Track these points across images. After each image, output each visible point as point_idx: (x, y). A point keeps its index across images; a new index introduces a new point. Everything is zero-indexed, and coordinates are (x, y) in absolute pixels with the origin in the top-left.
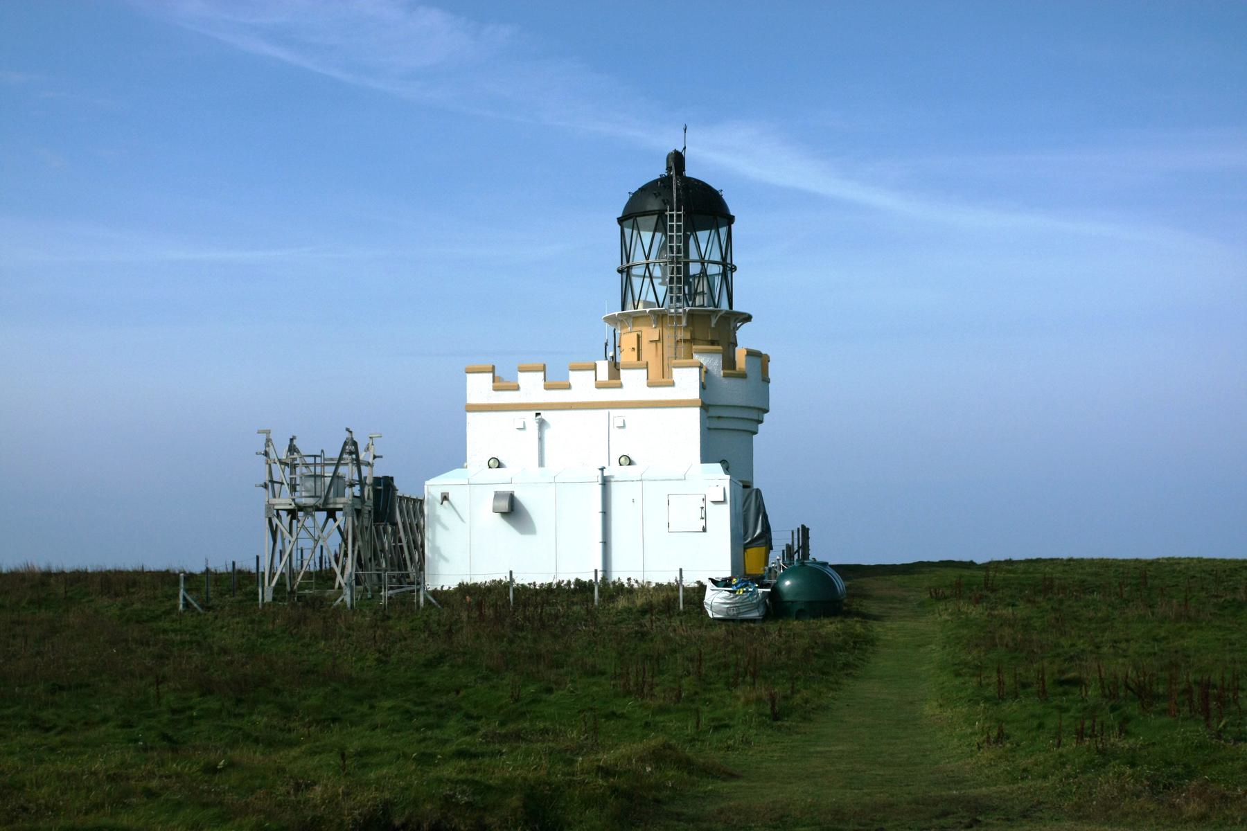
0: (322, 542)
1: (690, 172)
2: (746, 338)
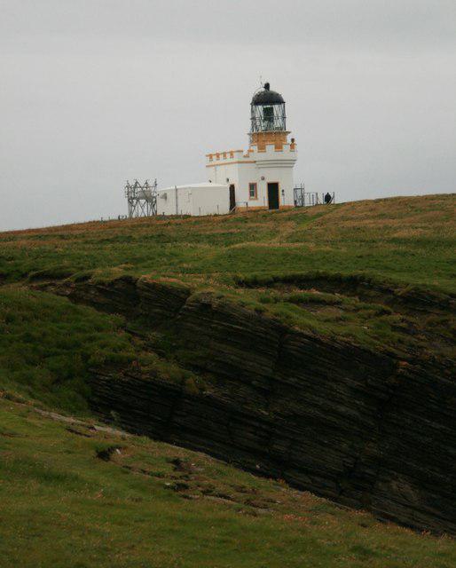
0: (142, 210)
1: (272, 89)
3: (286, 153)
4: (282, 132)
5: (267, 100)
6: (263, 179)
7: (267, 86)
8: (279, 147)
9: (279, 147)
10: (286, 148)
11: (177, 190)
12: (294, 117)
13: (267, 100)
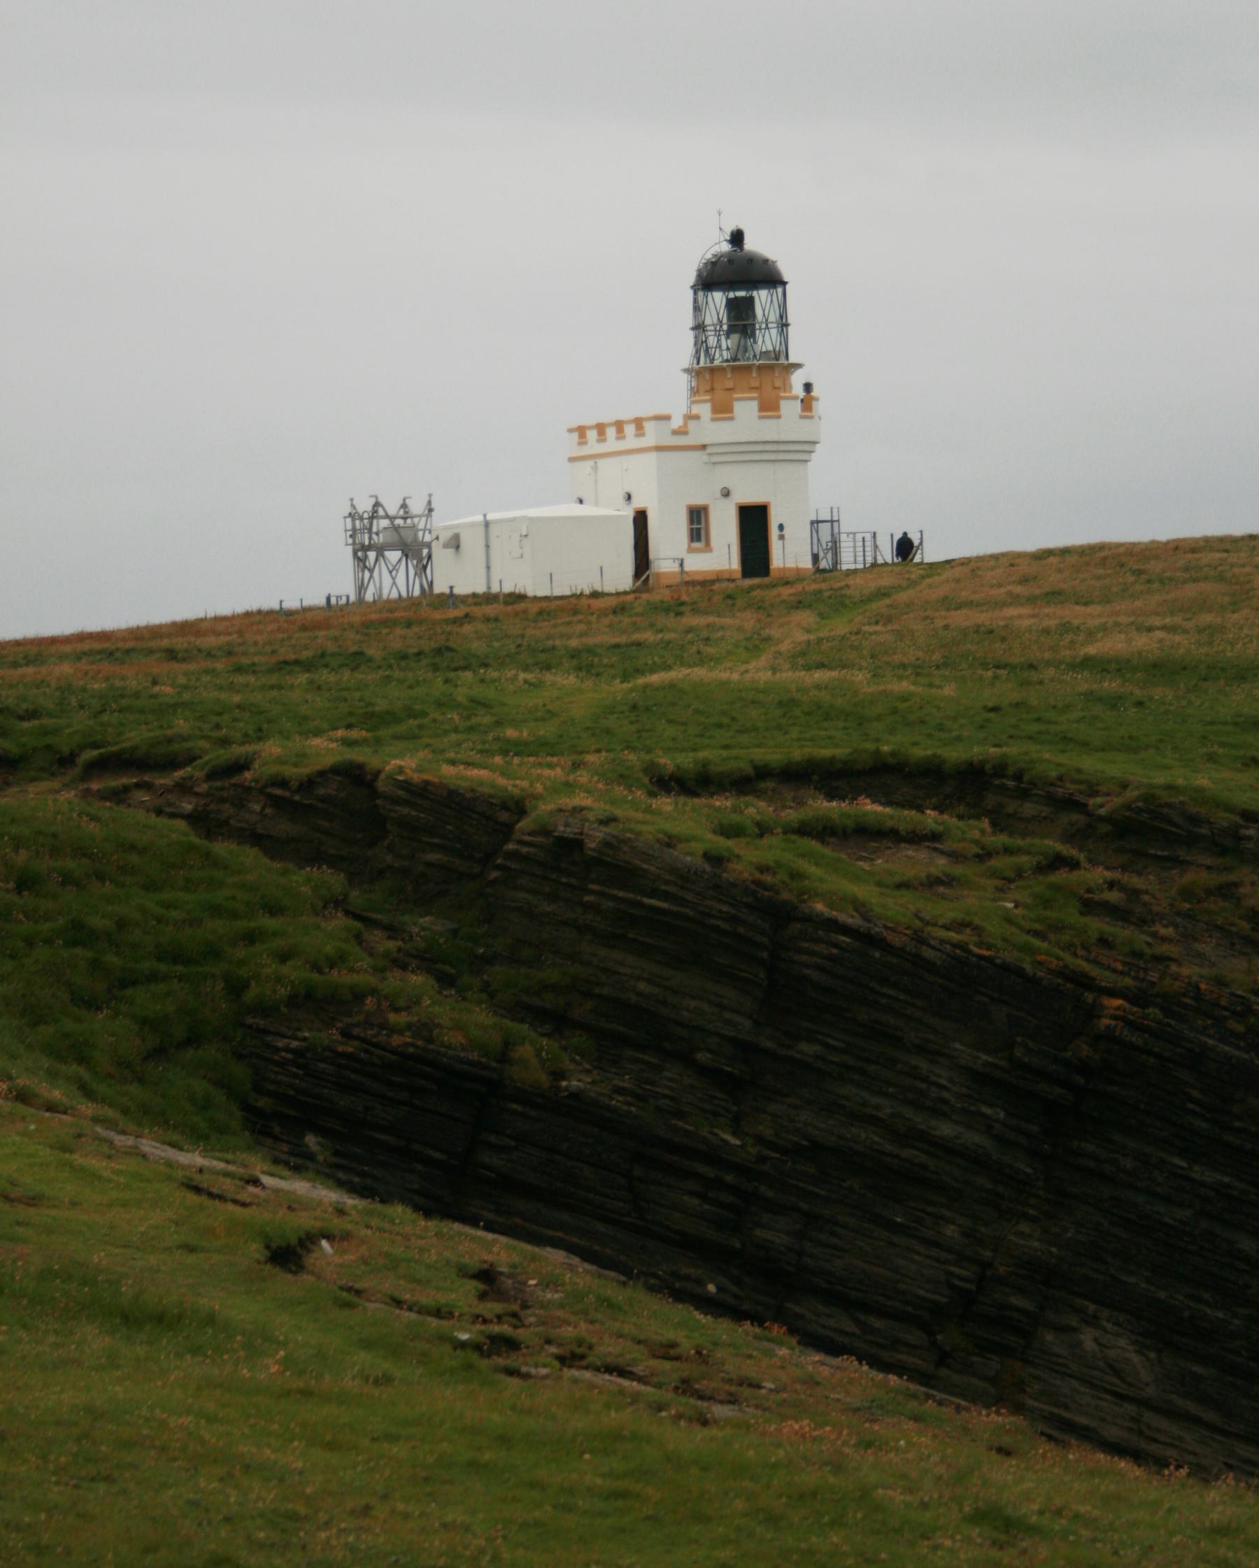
1: (750, 245)
2: (797, 381)
3: (789, 423)
4: (777, 366)
5: (738, 277)
6: (726, 494)
7: (737, 238)
8: (769, 407)
9: (769, 407)
10: (790, 409)
11: (487, 524)
12: (813, 324)
13: (738, 277)
